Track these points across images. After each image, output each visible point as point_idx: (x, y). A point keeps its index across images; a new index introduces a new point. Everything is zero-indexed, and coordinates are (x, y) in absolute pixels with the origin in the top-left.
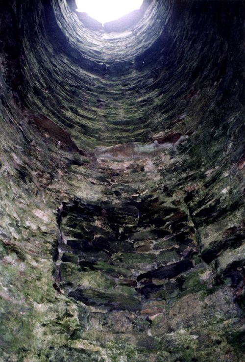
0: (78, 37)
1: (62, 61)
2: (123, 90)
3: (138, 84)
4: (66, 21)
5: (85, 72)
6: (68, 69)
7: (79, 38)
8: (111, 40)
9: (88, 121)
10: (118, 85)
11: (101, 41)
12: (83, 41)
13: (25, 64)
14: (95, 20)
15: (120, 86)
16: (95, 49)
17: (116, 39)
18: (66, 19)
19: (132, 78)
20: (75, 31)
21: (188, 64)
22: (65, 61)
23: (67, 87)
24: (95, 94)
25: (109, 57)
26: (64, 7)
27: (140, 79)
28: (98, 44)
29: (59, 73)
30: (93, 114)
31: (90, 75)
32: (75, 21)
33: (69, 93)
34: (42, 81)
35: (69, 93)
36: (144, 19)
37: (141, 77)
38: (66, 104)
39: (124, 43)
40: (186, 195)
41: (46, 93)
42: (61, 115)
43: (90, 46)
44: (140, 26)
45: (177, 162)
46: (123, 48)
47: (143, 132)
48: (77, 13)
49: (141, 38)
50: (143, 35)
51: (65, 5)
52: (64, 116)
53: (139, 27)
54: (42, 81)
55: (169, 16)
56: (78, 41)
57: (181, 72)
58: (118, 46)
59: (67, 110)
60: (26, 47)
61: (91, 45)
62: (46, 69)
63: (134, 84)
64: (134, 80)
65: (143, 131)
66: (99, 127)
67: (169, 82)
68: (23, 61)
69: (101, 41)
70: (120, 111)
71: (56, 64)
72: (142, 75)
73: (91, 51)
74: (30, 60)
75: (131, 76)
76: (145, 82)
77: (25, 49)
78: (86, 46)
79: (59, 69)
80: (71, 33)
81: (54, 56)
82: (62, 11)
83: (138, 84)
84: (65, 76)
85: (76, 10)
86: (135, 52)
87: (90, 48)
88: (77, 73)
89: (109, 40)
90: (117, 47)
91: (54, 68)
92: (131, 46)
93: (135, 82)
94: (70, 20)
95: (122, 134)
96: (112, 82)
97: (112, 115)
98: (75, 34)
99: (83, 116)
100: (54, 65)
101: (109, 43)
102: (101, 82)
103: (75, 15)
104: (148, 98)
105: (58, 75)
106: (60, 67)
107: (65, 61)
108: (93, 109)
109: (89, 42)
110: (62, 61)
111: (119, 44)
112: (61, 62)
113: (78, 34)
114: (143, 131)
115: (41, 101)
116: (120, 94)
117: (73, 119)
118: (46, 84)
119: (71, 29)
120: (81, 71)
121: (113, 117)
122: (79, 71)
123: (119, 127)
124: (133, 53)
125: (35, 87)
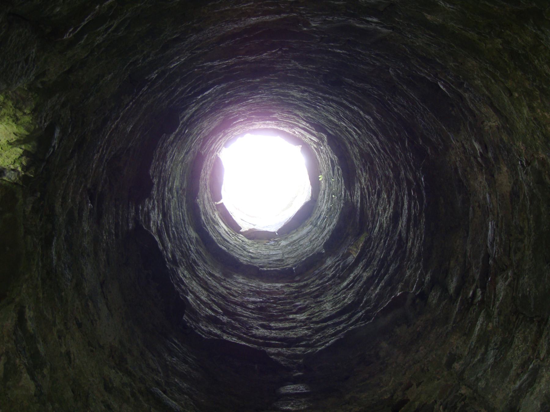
0: (250, 254)
1: (236, 282)
2: (322, 284)
3: (337, 269)
4: (231, 244)
5: (269, 284)
6: (247, 288)
7: (253, 255)
8: (292, 243)
9: (287, 332)
10: (313, 281)
11: (279, 249)
12: (258, 257)
13: (188, 293)
14: (223, 180)
15: (317, 281)
16: (275, 258)
17: (297, 240)
18: (231, 242)
19: (327, 267)
20: (245, 250)
21: (383, 218)
22: (241, 280)
23: (250, 306)
24: (289, 301)
25: (294, 260)
26: (224, 232)
27: (337, 263)
28: (277, 253)
29: (236, 295)
30: (292, 322)
31: (277, 285)
32: (243, 241)
33: (254, 311)
34: (215, 307)
35: (254, 311)
36: (320, 207)
37: (338, 261)
38: (255, 323)
39: (306, 240)
40: (452, 367)
41: (225, 319)
42: (251, 336)
43: (269, 258)
44: (318, 216)
45: (374, 272)
46: (307, 244)
47: (362, 315)
48: (242, 233)
49: (323, 226)
50: (325, 221)
51: (225, 230)
52: (254, 336)
53: (318, 217)
54: (215, 307)
55: (344, 187)
56: (252, 258)
57: (379, 230)
58: (301, 245)
59: (257, 329)
60: (184, 276)
61: (269, 256)
62: (219, 294)
63: (333, 271)
64: (331, 268)
65: (361, 314)
66: (304, 333)
67: (371, 248)
68: (183, 291)
69: (279, 249)
70: (325, 305)
71: (228, 286)
72: (338, 259)
73: (271, 262)
74: (193, 288)
75: (326, 266)
76: (344, 264)
77: (183, 279)
78: (263, 260)
79: (234, 291)
80: (242, 254)
81: (225, 280)
82: (223, 235)
83: (337, 269)
84: (244, 294)
85: (241, 231)
86: (322, 241)
87: (269, 260)
88: (259, 288)
89: (289, 245)
90: (300, 247)
91: (228, 291)
92: (316, 238)
93: (333, 269)
94: (235, 242)
95: (336, 329)
96: (305, 282)
97: (317, 314)
98: (245, 253)
99: (281, 329)
100: (227, 288)
101: (289, 248)
102: (292, 287)
103: (241, 235)
104: (354, 278)
105: (235, 297)
106: (235, 289)
107: (241, 280)
108: (291, 316)
109: (265, 255)
110: (236, 282)
111: (302, 243)
112: (236, 284)
113: (249, 252)
114: (361, 314)
115: (221, 329)
116: (319, 289)
117: (267, 336)
118: (222, 309)
119: (240, 249)
120: (264, 285)
121: (319, 315)
122: (262, 286)
123: (330, 323)
124: (320, 244)
125: (206, 315)
